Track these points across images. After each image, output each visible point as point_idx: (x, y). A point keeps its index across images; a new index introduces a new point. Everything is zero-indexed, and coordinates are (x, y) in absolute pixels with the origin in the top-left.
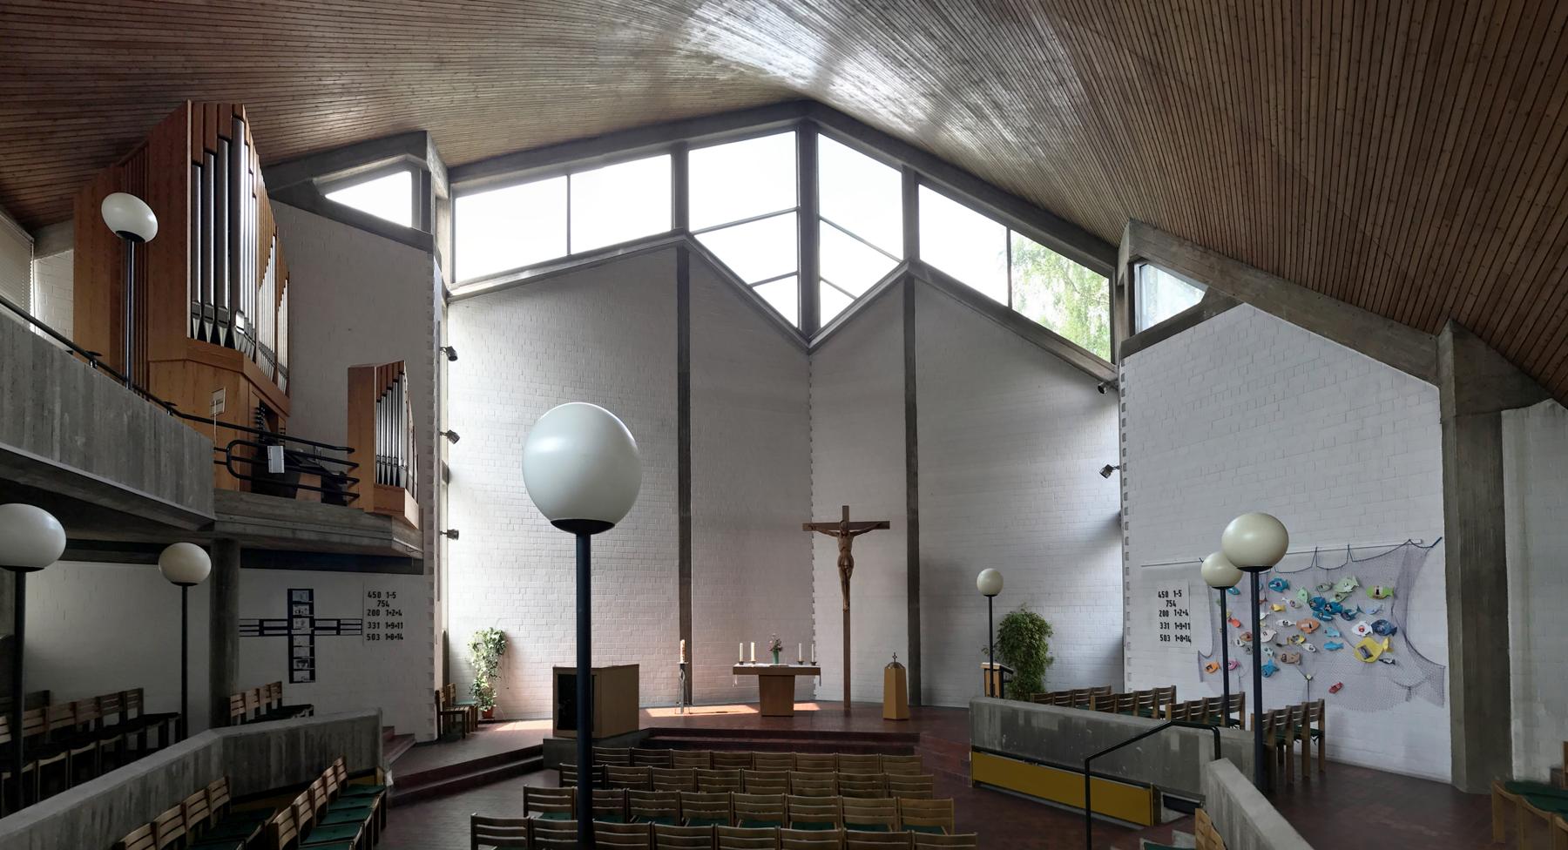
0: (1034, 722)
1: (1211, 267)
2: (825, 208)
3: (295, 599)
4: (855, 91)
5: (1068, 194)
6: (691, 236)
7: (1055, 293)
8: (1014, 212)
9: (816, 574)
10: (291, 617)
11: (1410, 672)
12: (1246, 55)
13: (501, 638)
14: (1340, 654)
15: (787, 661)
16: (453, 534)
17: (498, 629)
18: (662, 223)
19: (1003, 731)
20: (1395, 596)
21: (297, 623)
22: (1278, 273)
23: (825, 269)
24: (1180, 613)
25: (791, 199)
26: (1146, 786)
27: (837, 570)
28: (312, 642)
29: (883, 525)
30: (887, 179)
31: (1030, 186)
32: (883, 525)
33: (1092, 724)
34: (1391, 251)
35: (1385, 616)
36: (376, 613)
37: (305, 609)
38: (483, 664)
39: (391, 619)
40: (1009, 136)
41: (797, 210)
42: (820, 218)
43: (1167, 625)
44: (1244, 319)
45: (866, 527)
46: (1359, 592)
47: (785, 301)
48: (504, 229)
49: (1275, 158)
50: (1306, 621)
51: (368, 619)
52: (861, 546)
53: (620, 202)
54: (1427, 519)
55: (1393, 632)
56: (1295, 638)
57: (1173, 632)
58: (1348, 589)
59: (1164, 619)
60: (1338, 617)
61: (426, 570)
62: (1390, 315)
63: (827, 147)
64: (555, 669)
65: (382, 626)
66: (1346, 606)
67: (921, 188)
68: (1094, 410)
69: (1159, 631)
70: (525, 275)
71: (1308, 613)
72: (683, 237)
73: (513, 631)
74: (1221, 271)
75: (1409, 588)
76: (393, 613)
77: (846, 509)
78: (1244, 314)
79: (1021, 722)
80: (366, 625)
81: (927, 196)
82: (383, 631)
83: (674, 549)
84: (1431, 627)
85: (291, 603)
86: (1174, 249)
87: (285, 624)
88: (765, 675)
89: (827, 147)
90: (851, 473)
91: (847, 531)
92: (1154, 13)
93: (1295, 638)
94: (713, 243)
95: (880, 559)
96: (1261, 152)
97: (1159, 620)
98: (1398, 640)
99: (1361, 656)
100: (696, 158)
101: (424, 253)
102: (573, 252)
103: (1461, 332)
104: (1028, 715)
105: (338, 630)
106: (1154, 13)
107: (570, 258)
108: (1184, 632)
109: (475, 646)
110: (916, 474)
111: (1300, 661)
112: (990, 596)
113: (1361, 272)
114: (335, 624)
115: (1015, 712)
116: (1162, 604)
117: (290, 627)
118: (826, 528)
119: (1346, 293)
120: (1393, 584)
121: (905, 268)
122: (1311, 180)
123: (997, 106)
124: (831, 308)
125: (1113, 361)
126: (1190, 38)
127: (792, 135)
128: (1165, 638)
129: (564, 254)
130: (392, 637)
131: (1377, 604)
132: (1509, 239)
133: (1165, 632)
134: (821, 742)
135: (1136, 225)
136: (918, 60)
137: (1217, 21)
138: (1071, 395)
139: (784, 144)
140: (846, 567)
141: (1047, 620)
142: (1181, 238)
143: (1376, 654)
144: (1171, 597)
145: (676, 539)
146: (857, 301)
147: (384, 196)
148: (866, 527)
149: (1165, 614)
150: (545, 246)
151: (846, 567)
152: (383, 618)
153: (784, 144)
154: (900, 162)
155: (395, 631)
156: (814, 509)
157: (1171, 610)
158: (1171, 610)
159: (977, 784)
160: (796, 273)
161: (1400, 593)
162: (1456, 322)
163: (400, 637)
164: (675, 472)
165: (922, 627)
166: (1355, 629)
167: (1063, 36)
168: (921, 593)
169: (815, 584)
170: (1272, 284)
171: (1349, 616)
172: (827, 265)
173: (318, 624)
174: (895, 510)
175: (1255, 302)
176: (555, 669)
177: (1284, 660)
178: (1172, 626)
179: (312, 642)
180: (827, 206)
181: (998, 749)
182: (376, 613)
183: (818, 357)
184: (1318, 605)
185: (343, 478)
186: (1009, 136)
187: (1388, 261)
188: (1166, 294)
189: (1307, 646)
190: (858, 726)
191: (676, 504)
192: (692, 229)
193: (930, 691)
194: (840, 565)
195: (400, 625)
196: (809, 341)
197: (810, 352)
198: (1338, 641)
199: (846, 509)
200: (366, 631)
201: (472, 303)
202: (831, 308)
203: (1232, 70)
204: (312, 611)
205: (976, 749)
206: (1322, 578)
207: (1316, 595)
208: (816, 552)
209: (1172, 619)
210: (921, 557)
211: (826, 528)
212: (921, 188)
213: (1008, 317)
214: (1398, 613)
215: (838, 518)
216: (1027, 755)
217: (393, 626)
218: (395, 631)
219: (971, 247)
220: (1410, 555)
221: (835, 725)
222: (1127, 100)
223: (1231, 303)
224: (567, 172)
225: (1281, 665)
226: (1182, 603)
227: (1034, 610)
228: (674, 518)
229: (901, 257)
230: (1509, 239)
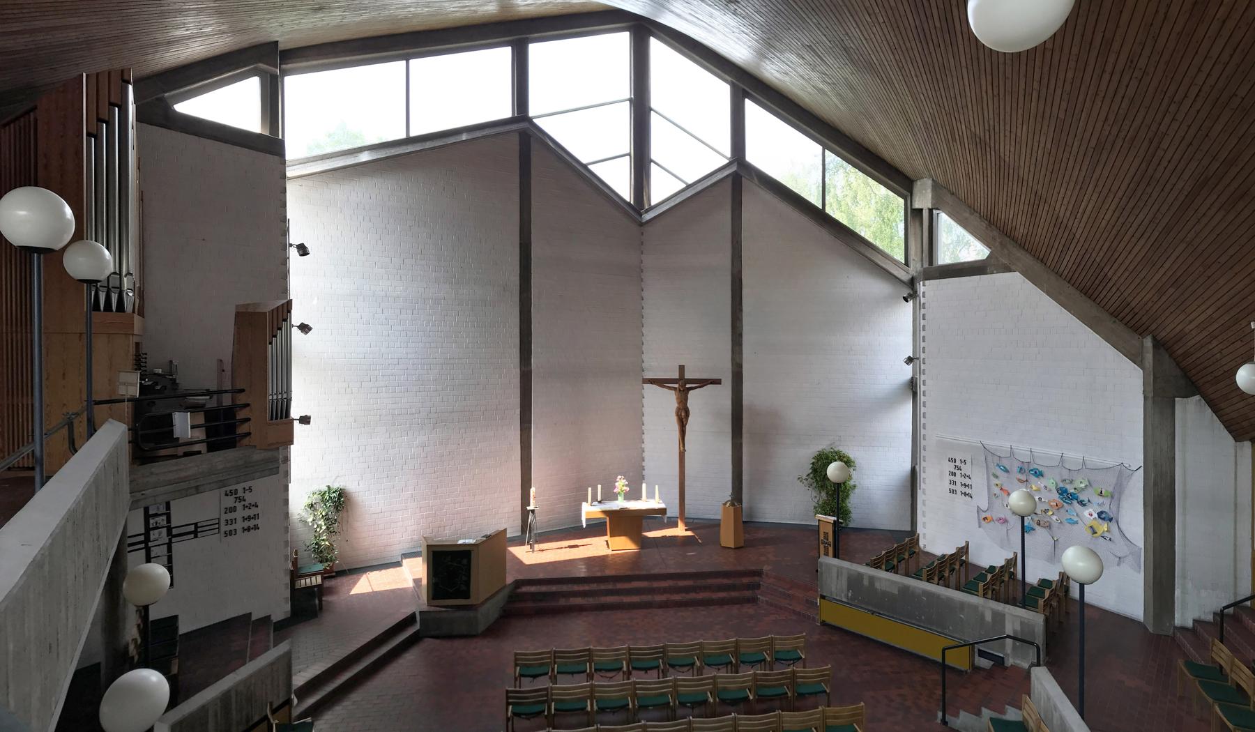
0: (877, 585)
1: (994, 238)
2: (655, 102)
3: (151, 512)
5: (881, 145)
6: (530, 120)
7: (865, 204)
10: (148, 529)
11: (1120, 548)
13: (340, 495)
14: (1075, 527)
16: (305, 420)
17: (335, 486)
18: (505, 111)
20: (1112, 497)
21: (154, 535)
24: (965, 476)
25: (624, 89)
27: (674, 419)
28: (170, 550)
30: (720, 90)
32: (717, 382)
33: (925, 593)
34: (1122, 289)
35: (1106, 509)
36: (233, 510)
37: (162, 521)
38: (321, 522)
39: (248, 513)
41: (630, 100)
42: (651, 109)
43: (954, 483)
44: (1014, 284)
45: (702, 383)
46: (1090, 489)
47: (619, 179)
48: (333, 112)
51: (224, 517)
53: (462, 91)
54: (1135, 456)
55: (1111, 520)
56: (1046, 511)
57: (958, 488)
58: (1082, 485)
59: (952, 478)
60: (1075, 502)
62: (1115, 314)
63: (658, 49)
65: (239, 520)
66: (1081, 497)
67: (747, 101)
69: (947, 486)
70: (365, 157)
71: (1056, 496)
72: (522, 125)
73: (351, 485)
74: (1001, 243)
75: (1120, 494)
76: (250, 506)
77: (682, 368)
78: (1014, 280)
79: (866, 582)
80: (223, 523)
81: (750, 106)
82: (240, 525)
84: (1133, 520)
85: (147, 516)
86: (967, 215)
87: (142, 538)
89: (658, 49)
91: (683, 386)
93: (1046, 511)
97: (948, 478)
98: (1113, 526)
99: (1090, 531)
100: (537, 51)
101: (277, 158)
102: (413, 133)
103: (1157, 344)
104: (872, 579)
105: (195, 534)
107: (409, 141)
108: (967, 490)
109: (311, 506)
110: (741, 335)
111: (1049, 526)
113: (1100, 288)
114: (192, 528)
115: (860, 576)
116: (951, 467)
117: (147, 540)
119: (1089, 293)
120: (1111, 489)
121: (734, 168)
122: (1078, 236)
124: (662, 189)
125: (907, 264)
127: (627, 34)
128: (952, 491)
129: (403, 136)
130: (249, 529)
131: (1101, 500)
132: (1190, 318)
133: (953, 487)
135: (936, 187)
138: (875, 287)
139: (619, 42)
140: (683, 416)
141: (851, 456)
142: (973, 209)
143: (1099, 532)
144: (958, 463)
146: (689, 186)
147: (233, 104)
148: (702, 383)
149: (954, 474)
151: (683, 416)
152: (240, 513)
153: (619, 42)
154: (729, 79)
155: (252, 523)
156: (645, 357)
157: (958, 473)
158: (958, 473)
159: (824, 623)
160: (629, 154)
161: (1116, 495)
162: (1154, 339)
163: (256, 527)
164: (517, 331)
166: (1086, 513)
169: (645, 418)
170: (1038, 267)
171: (1081, 503)
172: (658, 149)
173: (175, 532)
175: (1025, 274)
177: (1039, 524)
178: (958, 484)
179: (170, 550)
182: (233, 510)
184: (1062, 492)
185: (230, 412)
187: (1118, 293)
188: (958, 243)
189: (1054, 518)
192: (531, 114)
193: (751, 509)
194: (678, 415)
195: (256, 516)
197: (642, 224)
198: (1075, 519)
199: (682, 368)
200: (224, 528)
201: (300, 181)
202: (662, 189)
204: (169, 520)
205: (823, 597)
206: (1066, 475)
207: (1061, 485)
209: (958, 479)
210: (745, 403)
212: (747, 101)
213: (819, 216)
214: (1114, 508)
215: (676, 376)
217: (249, 518)
218: (252, 523)
220: (1122, 474)
222: (954, 140)
223: (1007, 269)
224: (407, 58)
225: (1037, 527)
226: (966, 469)
227: (841, 449)
228: (516, 372)
229: (729, 155)
230: (1190, 318)
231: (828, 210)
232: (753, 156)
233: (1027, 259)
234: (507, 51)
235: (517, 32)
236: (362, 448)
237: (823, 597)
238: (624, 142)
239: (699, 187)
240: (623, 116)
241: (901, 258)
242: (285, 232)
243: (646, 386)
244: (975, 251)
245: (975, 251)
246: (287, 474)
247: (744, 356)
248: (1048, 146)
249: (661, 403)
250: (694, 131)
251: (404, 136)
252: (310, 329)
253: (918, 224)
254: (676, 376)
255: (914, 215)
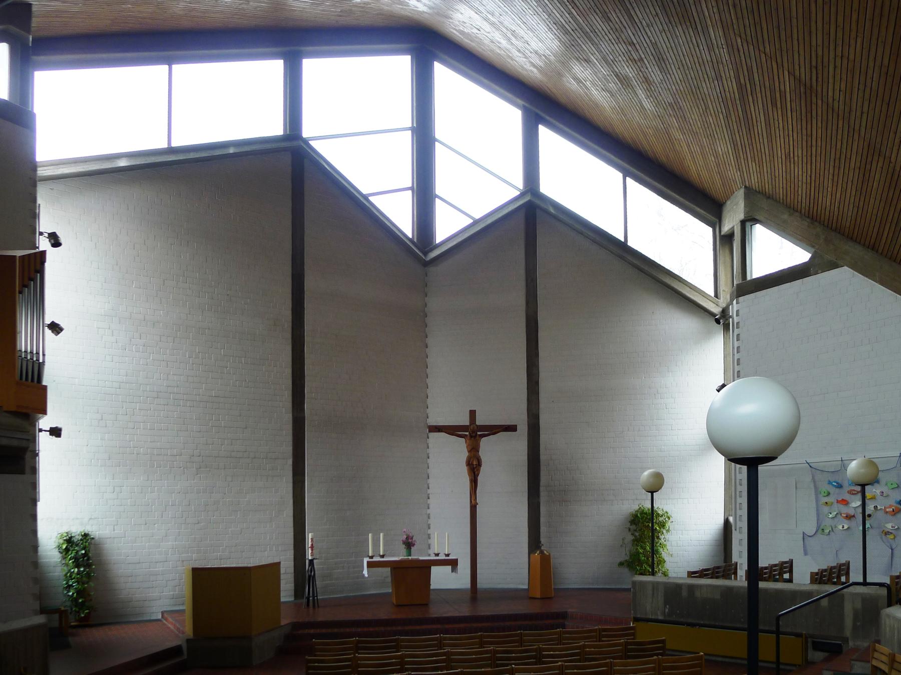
0: (698, 594)
4: (504, 43)
7: (675, 239)
8: (631, 162)
9: (433, 471)
12: (887, 98)
15: (418, 555)
19: (666, 603)
22: (873, 248)
23: (441, 186)
25: (405, 116)
26: (798, 635)
27: (465, 469)
29: (512, 428)
30: (508, 116)
31: (655, 146)
32: (512, 428)
40: (647, 104)
41: (412, 189)
42: (435, 140)
44: (844, 280)
45: (493, 430)
47: (400, 214)
48: (91, 113)
49: (891, 170)
50: (890, 506)
52: (488, 447)
53: (223, 101)
61: (27, 469)
64: (197, 573)
68: (709, 334)
70: (123, 163)
77: (473, 413)
78: (844, 275)
79: (684, 593)
81: (545, 134)
83: (288, 449)
86: (786, 216)
88: (398, 569)
90: (462, 376)
91: (473, 433)
92: (820, 53)
94: (323, 148)
95: (503, 457)
96: (880, 164)
102: (175, 144)
106: (820, 53)
110: (537, 383)
112: (652, 493)
118: (452, 430)
123: (646, 80)
124: (447, 226)
125: (716, 295)
126: (844, 77)
134: (324, 631)
135: (750, 193)
136: (586, 33)
137: (870, 72)
139: (399, 66)
142: (792, 209)
145: (289, 438)
146: (476, 222)
148: (493, 430)
150: (143, 135)
151: (474, 466)
153: (399, 66)
164: (288, 371)
165: (542, 520)
167: (730, 46)
168: (542, 489)
169: (431, 481)
174: (519, 416)
175: (854, 267)
176: (197, 573)
180: (441, 128)
181: (661, 618)
183: (432, 269)
186: (647, 104)
188: (772, 251)
190: (485, 610)
191: (289, 405)
192: (305, 134)
194: (469, 463)
196: (426, 254)
197: (426, 264)
199: (473, 413)
201: (58, 186)
202: (447, 226)
203: (872, 105)
205: (636, 620)
208: (432, 451)
211: (452, 430)
215: (466, 422)
216: (690, 621)
219: (587, 185)
221: (464, 611)
222: (774, 104)
223: (834, 266)
224: (171, 150)
228: (288, 417)
229: (521, 186)
231: (630, 243)
232: (549, 187)
233: (857, 251)
234: (278, 65)
235: (289, 39)
236: (117, 489)
237: (636, 620)
238: (405, 176)
239: (489, 221)
240: (405, 144)
241: (711, 292)
242: (34, 216)
243: (432, 435)
244: (799, 256)
245: (799, 256)
246: (34, 471)
247: (542, 406)
248: (886, 62)
249: (448, 455)
250: (485, 161)
251: (165, 146)
252: (61, 330)
253: (727, 251)
254: (466, 422)
255: (724, 241)
